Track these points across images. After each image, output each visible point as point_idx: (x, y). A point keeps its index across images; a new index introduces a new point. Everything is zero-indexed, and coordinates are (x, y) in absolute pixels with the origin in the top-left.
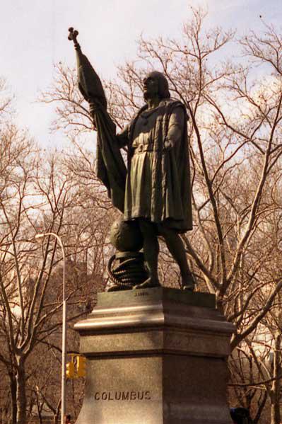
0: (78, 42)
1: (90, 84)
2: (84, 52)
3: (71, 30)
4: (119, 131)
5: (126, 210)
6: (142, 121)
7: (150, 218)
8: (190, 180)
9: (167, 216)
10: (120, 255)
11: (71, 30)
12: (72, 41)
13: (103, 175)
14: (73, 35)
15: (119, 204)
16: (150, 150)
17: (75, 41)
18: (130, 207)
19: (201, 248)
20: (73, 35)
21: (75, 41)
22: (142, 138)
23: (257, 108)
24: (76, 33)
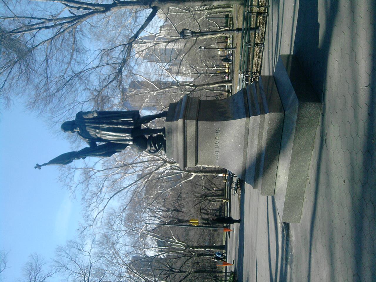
0: (42, 164)
1: (65, 159)
2: (48, 162)
3: (36, 168)
4: (88, 146)
5: (128, 142)
6: (84, 134)
7: (132, 128)
8: (120, 118)
9: (132, 119)
10: (149, 148)
11: (36, 168)
12: (41, 167)
13: (109, 154)
14: (38, 166)
15: (124, 146)
16: (99, 128)
17: (42, 166)
18: (126, 140)
19: (49, 6)
20: (38, 166)
21: (42, 166)
22: (92, 132)
23: (102, 216)
24: (37, 165)
